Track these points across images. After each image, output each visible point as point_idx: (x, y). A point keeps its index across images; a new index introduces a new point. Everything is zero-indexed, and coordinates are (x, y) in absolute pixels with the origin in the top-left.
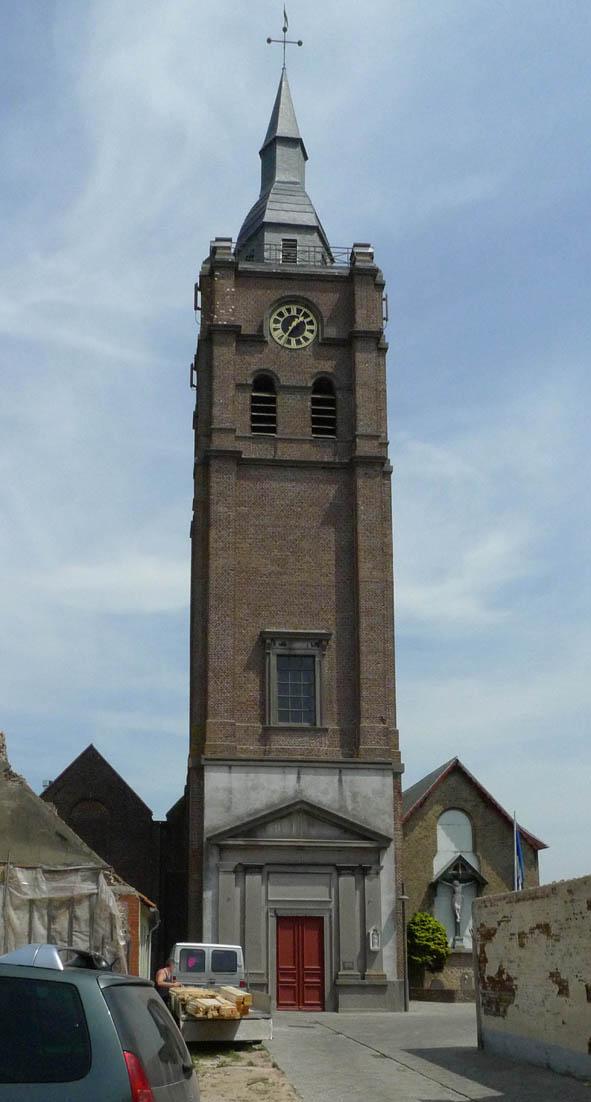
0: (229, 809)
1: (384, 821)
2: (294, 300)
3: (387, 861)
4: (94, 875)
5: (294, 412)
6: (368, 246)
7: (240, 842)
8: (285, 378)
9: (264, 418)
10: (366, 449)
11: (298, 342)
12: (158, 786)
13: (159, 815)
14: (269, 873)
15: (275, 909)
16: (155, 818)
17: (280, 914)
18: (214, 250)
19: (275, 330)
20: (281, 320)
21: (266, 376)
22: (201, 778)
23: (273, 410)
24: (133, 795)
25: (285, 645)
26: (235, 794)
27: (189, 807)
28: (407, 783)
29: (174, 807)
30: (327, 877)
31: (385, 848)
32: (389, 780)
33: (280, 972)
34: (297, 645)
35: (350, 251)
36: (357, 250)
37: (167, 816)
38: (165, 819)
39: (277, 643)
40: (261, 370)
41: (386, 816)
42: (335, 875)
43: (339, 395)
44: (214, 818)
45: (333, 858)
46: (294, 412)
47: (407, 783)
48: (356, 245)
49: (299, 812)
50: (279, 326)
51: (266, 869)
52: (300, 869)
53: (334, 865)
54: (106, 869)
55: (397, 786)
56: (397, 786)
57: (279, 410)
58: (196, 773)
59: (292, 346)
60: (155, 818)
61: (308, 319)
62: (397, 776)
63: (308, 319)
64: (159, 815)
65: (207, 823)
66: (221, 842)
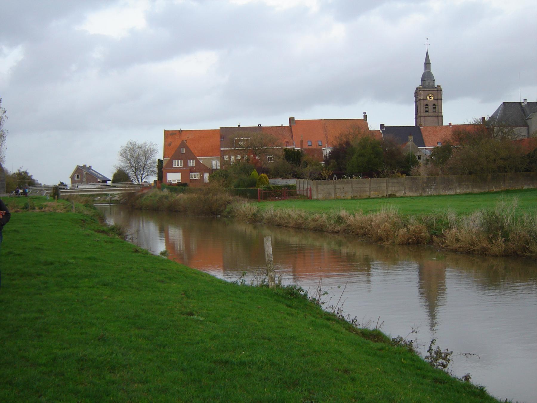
5: (431, 108)
8: (429, 104)
46: (431, 108)
59: (430, 100)
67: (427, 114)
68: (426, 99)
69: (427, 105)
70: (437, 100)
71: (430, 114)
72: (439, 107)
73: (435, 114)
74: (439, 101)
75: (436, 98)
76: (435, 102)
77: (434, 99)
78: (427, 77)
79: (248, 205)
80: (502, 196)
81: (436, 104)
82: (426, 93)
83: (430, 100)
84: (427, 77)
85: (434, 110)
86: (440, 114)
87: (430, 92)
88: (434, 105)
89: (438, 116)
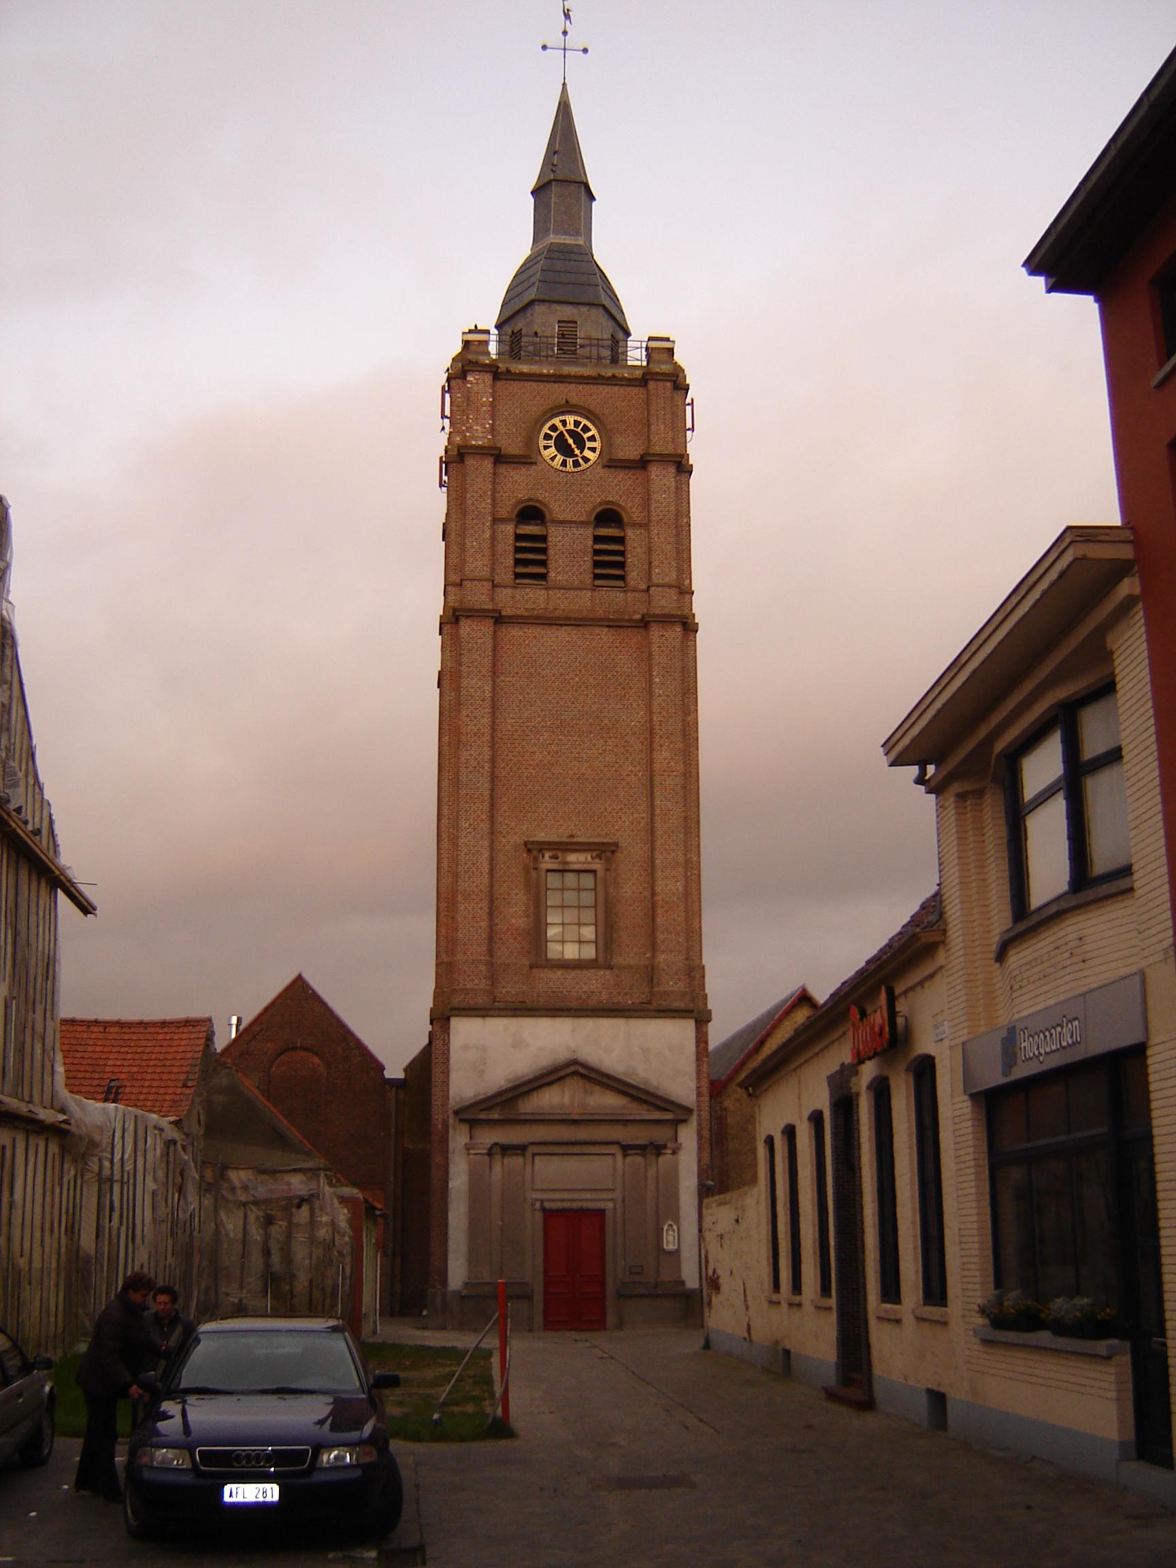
0: (482, 1072)
1: (681, 1084)
2: (569, 408)
3: (688, 1137)
4: (312, 1173)
5: (569, 548)
6: (667, 340)
7: (495, 1115)
8: (557, 509)
9: (531, 559)
10: (664, 603)
11: (553, 428)
12: (391, 1029)
13: (394, 1070)
14: (534, 1155)
15: (542, 1201)
16: (388, 1074)
17: (547, 1205)
18: (466, 344)
19: (546, 448)
20: (554, 435)
21: (535, 507)
22: (446, 1030)
23: (544, 551)
24: (359, 1044)
25: (557, 858)
26: (496, 1052)
27: (428, 1067)
28: (718, 1034)
29: (414, 1059)
30: (609, 1159)
31: (685, 1121)
32: (689, 1026)
33: (548, 1281)
34: (572, 857)
35: (644, 345)
36: (653, 344)
37: (405, 1070)
38: (401, 1075)
39: (547, 855)
40: (530, 499)
41: (518, 597)
42: (619, 1157)
43: (630, 533)
44: (464, 1083)
45: (618, 1133)
46: (569, 548)
47: (718, 1034)
48: (650, 339)
49: (575, 1073)
50: (551, 442)
51: (531, 1150)
52: (576, 1149)
53: (617, 1143)
54: (329, 1170)
55: (701, 1039)
56: (701, 1039)
57: (551, 552)
58: (441, 1018)
59: (569, 476)
60: (388, 1074)
61: (589, 434)
62: (702, 1019)
63: (589, 434)
64: (394, 1070)
65: (452, 1092)
66: (475, 1114)
67: (533, 598)
68: (527, 459)
69: (531, 513)
70: (642, 463)
71: (561, 602)
72: (661, 537)
73: (612, 599)
74: (660, 476)
75: (629, 450)
76: (619, 490)
77: (611, 463)
78: (562, 286)
79: (566, 1100)
80: (478, 457)
81: (632, 510)
82: (536, 396)
83: (569, 476)
84: (562, 286)
85: (609, 565)
86: (664, 602)
87: (572, 393)
88: (608, 516)
89: (644, 624)
